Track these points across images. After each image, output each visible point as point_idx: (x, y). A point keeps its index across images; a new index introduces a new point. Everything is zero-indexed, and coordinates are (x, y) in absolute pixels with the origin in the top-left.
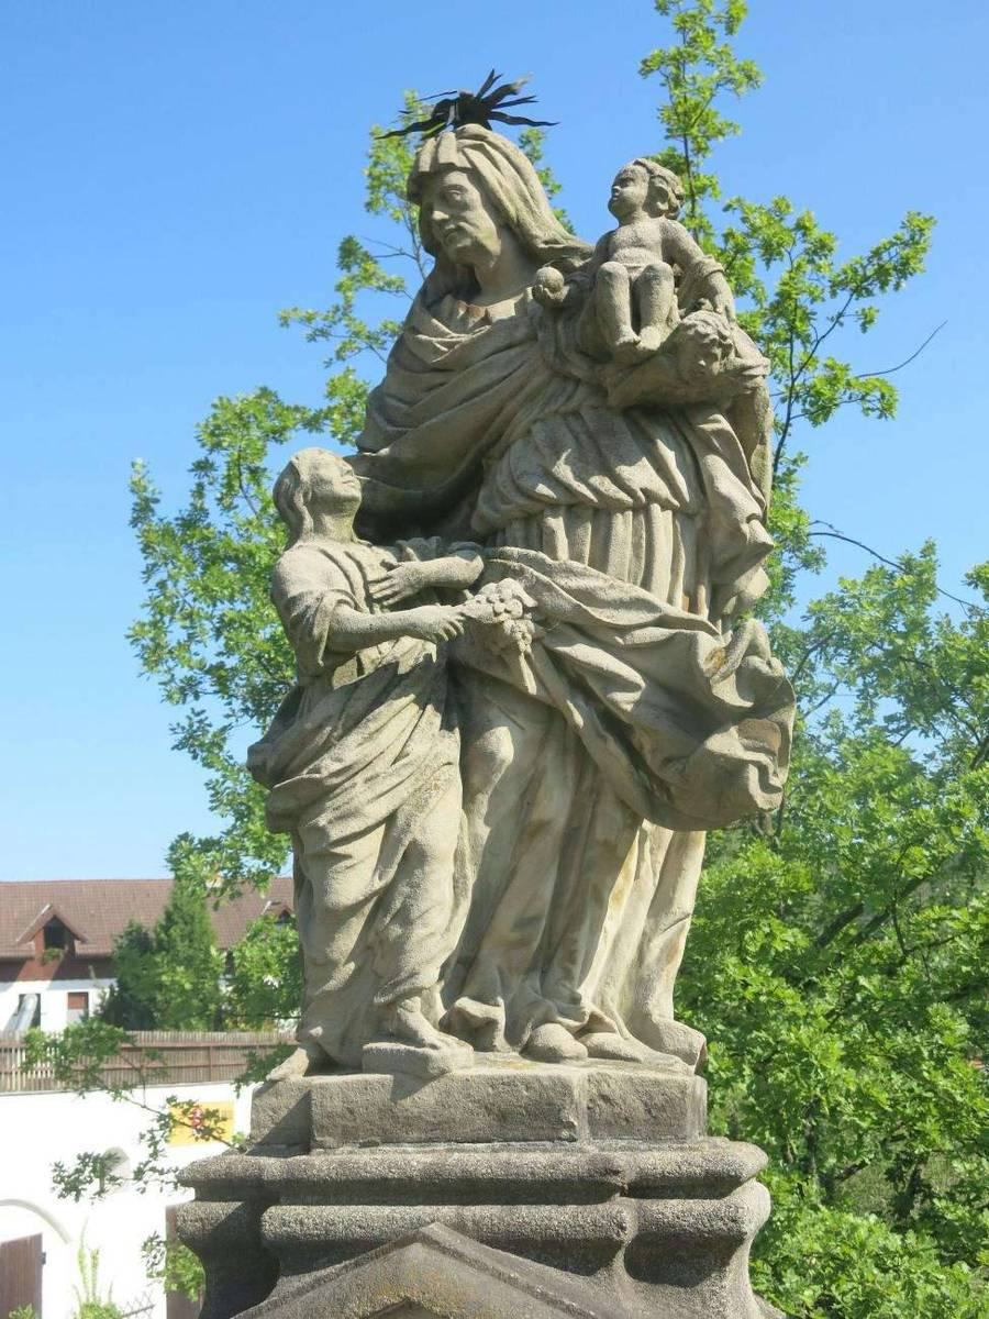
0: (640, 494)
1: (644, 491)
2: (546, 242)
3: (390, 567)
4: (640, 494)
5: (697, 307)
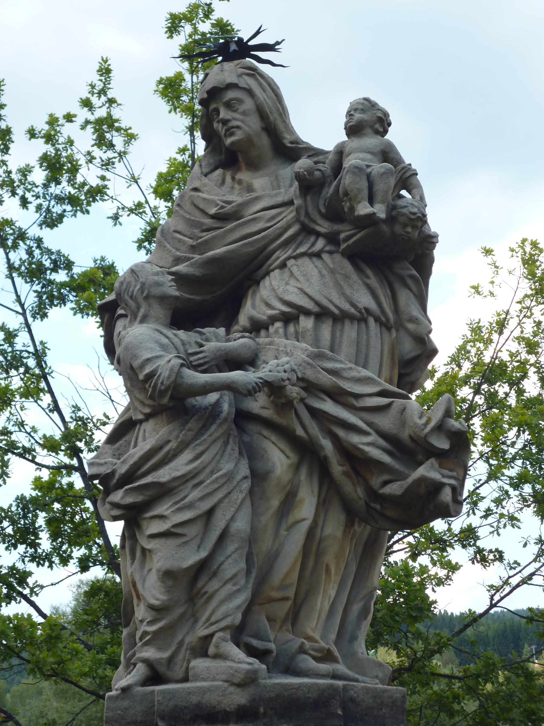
1: (366, 309)
2: (292, 143)
3: (201, 346)
4: (364, 311)
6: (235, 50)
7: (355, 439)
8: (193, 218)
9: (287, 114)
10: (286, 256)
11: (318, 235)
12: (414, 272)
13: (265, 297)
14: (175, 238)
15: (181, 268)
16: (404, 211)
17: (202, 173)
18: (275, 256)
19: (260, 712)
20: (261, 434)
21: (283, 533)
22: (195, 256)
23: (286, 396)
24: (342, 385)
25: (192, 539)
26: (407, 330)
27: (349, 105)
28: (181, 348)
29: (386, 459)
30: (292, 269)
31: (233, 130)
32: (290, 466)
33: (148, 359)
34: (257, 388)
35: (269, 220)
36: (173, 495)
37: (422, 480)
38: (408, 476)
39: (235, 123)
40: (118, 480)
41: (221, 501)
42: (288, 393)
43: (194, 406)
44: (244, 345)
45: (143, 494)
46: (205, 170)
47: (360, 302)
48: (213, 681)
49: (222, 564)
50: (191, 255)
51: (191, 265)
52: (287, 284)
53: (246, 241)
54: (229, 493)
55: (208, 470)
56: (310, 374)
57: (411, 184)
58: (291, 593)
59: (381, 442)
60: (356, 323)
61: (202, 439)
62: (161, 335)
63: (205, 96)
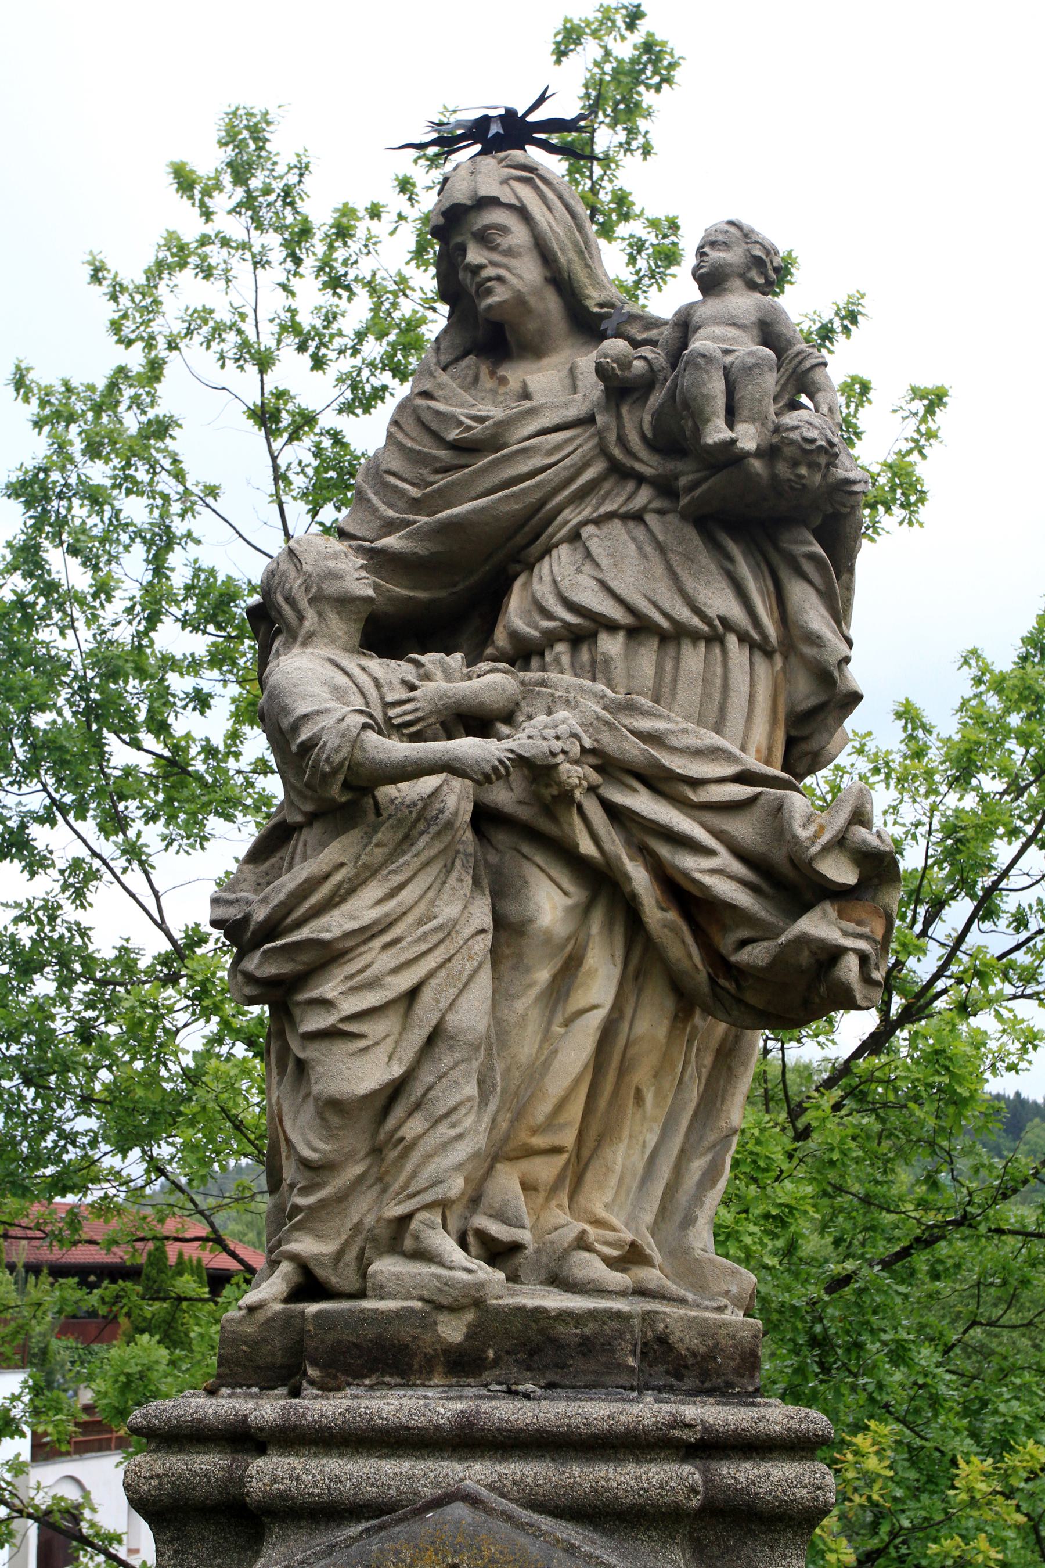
0: (717, 623)
1: (723, 620)
2: (601, 305)
3: (412, 688)
4: (717, 623)
5: (795, 406)
6: (498, 133)
7: (689, 862)
8: (418, 448)
9: (594, 251)
10: (579, 518)
11: (640, 479)
12: (818, 549)
13: (539, 595)
14: (386, 485)
15: (392, 542)
16: (794, 435)
17: (438, 362)
18: (560, 519)
19: (487, 1358)
20: (519, 851)
21: (557, 1029)
22: (419, 518)
23: (559, 784)
24: (667, 764)
25: (377, 1044)
26: (802, 657)
27: (703, 234)
28: (373, 694)
29: (743, 898)
30: (588, 544)
31: (489, 284)
32: (569, 910)
33: (305, 716)
34: (502, 770)
35: (549, 453)
36: (350, 960)
37: (803, 940)
38: (783, 931)
39: (490, 272)
40: (253, 933)
41: (431, 974)
42: (564, 777)
43: (392, 801)
44: (493, 686)
45: (293, 960)
46: (444, 358)
47: (710, 606)
48: (406, 1299)
49: (430, 1088)
50: (412, 517)
51: (410, 536)
52: (578, 571)
53: (507, 492)
54: (449, 960)
55: (411, 918)
56: (609, 742)
57: (813, 383)
58: (568, 1138)
59: (737, 867)
60: (702, 646)
61: (401, 861)
62: (336, 670)
63: (441, 220)
